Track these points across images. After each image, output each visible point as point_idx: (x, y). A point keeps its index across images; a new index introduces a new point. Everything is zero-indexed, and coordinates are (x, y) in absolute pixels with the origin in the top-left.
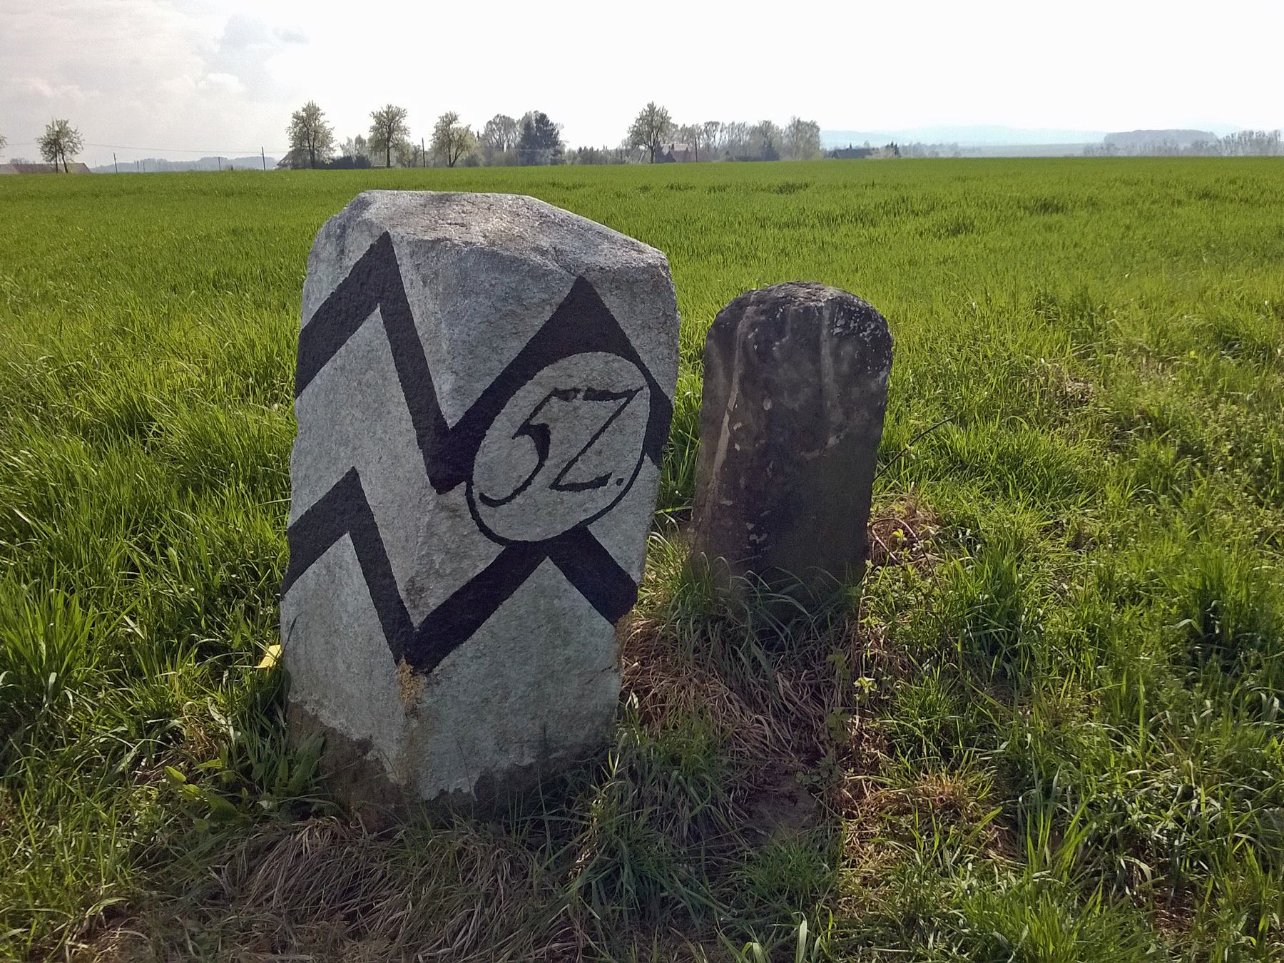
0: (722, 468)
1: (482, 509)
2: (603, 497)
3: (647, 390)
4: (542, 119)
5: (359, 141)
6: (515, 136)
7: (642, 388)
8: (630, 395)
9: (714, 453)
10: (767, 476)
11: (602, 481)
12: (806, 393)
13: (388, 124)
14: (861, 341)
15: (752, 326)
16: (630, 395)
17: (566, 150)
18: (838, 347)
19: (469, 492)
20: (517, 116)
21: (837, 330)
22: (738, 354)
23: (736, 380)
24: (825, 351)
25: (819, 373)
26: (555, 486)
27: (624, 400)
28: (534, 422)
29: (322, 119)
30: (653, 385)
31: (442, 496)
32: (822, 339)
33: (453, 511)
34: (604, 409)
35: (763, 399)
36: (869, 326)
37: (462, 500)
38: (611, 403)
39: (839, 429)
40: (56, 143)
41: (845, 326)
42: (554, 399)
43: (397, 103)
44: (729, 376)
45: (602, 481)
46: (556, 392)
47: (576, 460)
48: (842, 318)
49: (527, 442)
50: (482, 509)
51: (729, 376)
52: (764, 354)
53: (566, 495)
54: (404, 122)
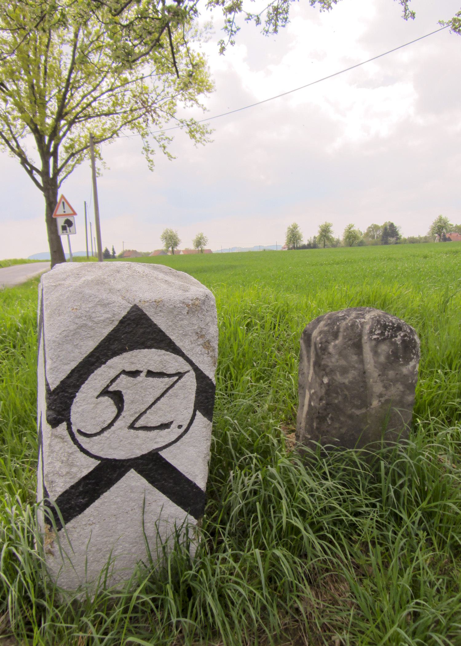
0: (306, 416)
1: (80, 438)
2: (172, 434)
3: (192, 373)
4: (392, 225)
5: (315, 238)
6: (380, 233)
7: (188, 371)
8: (180, 375)
9: (303, 406)
10: (328, 423)
11: (165, 426)
12: (352, 375)
13: (325, 232)
14: (395, 343)
15: (320, 333)
16: (180, 375)
17: (402, 238)
18: (376, 346)
19: (69, 428)
20: (381, 224)
21: (375, 337)
22: (312, 349)
23: (312, 364)
24: (367, 349)
25: (362, 361)
26: (132, 426)
27: (176, 378)
28: (111, 389)
29: (298, 228)
30: (196, 369)
31: (54, 430)
32: (363, 341)
33: (62, 438)
34: (162, 383)
35: (323, 376)
36: (400, 334)
37: (66, 433)
38: (166, 380)
39: (381, 396)
40: (199, 242)
41: (382, 334)
42: (123, 376)
43: (329, 222)
44: (309, 361)
45: (165, 426)
46: (124, 372)
47: (145, 412)
48: (379, 329)
49: (107, 401)
50: (80, 438)
51: (309, 361)
52: (324, 349)
53: (141, 433)
54: (331, 229)
